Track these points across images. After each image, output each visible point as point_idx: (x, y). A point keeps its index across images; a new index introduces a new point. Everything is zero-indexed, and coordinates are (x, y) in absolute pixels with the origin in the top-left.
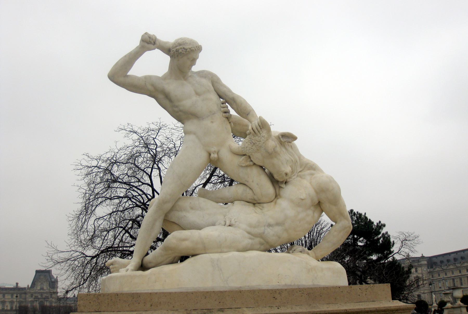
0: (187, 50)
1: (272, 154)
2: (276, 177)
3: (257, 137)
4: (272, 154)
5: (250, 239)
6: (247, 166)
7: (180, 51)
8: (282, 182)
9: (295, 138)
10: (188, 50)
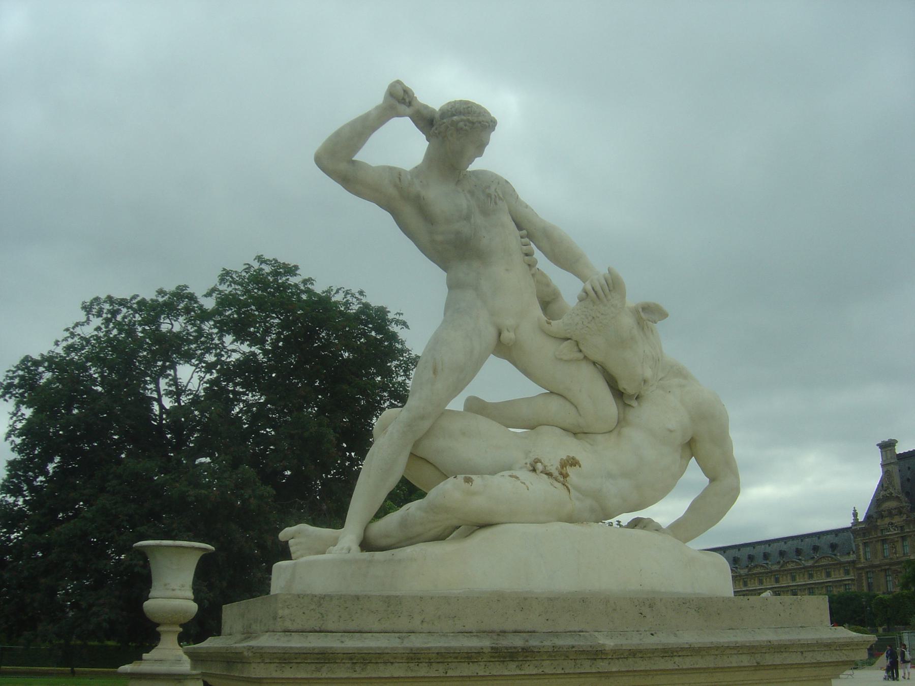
2: (623, 385)
7: (461, 124)
9: (663, 315)
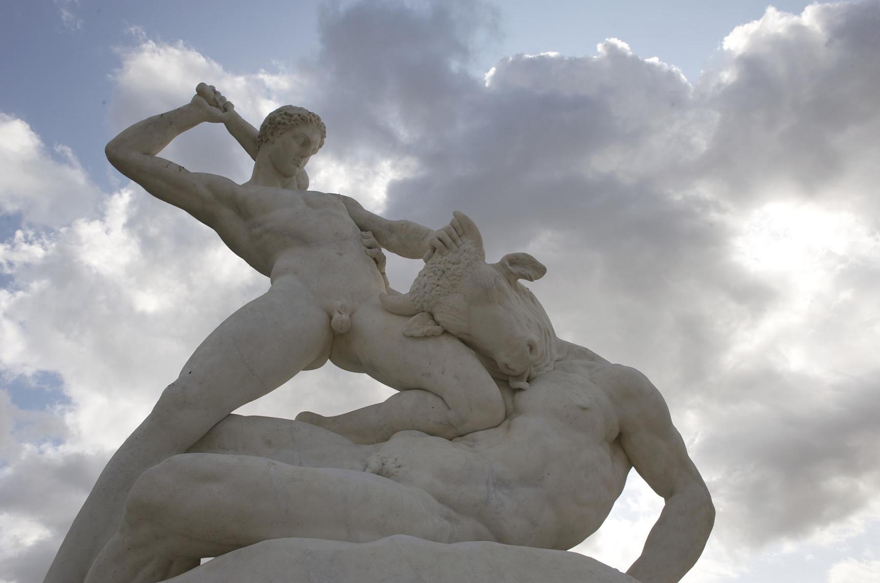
0: (291, 116)
1: (486, 295)
3: (451, 254)
4: (486, 295)
5: (448, 518)
6: (426, 337)
8: (518, 377)
10: (296, 116)
